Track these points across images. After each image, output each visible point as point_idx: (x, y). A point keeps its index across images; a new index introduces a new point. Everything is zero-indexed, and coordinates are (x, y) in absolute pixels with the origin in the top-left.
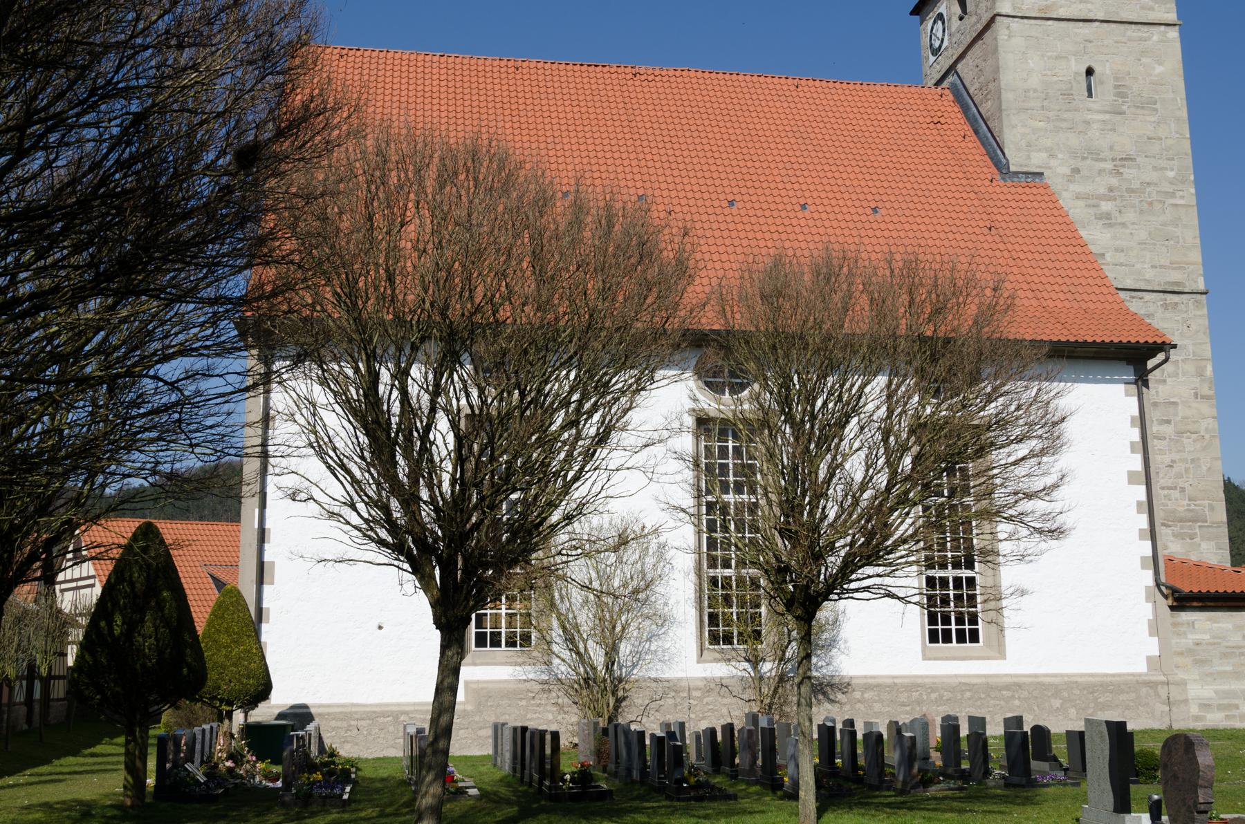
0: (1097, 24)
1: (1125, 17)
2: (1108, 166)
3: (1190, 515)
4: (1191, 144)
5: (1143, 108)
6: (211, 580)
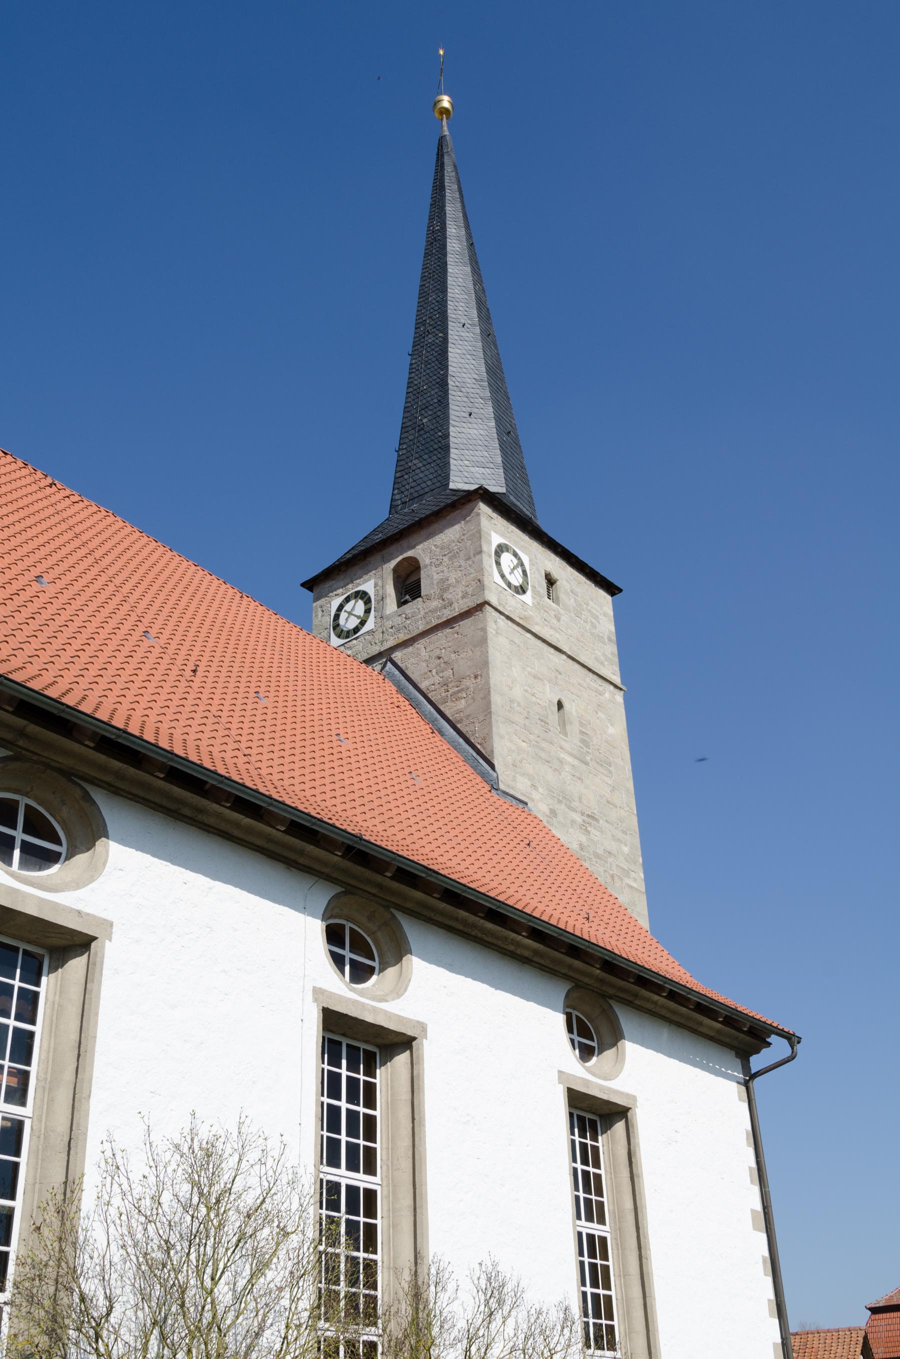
0: (564, 657)
1: (582, 659)
2: (578, 818)
3: (420, 1283)
5: (601, 765)
6: (861, 1340)
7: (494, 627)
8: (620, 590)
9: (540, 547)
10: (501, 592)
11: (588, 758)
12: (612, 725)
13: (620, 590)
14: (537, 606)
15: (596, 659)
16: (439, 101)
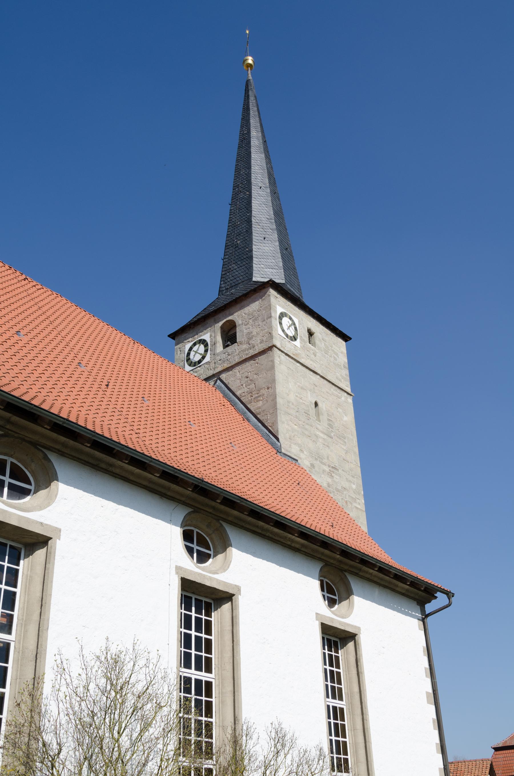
0: (318, 377)
3: (237, 735)
4: (361, 471)
5: (340, 438)
7: (279, 360)
8: (350, 339)
9: (305, 314)
11: (332, 434)
12: (346, 415)
13: (350, 339)
14: (303, 347)
15: (337, 378)
16: (247, 60)
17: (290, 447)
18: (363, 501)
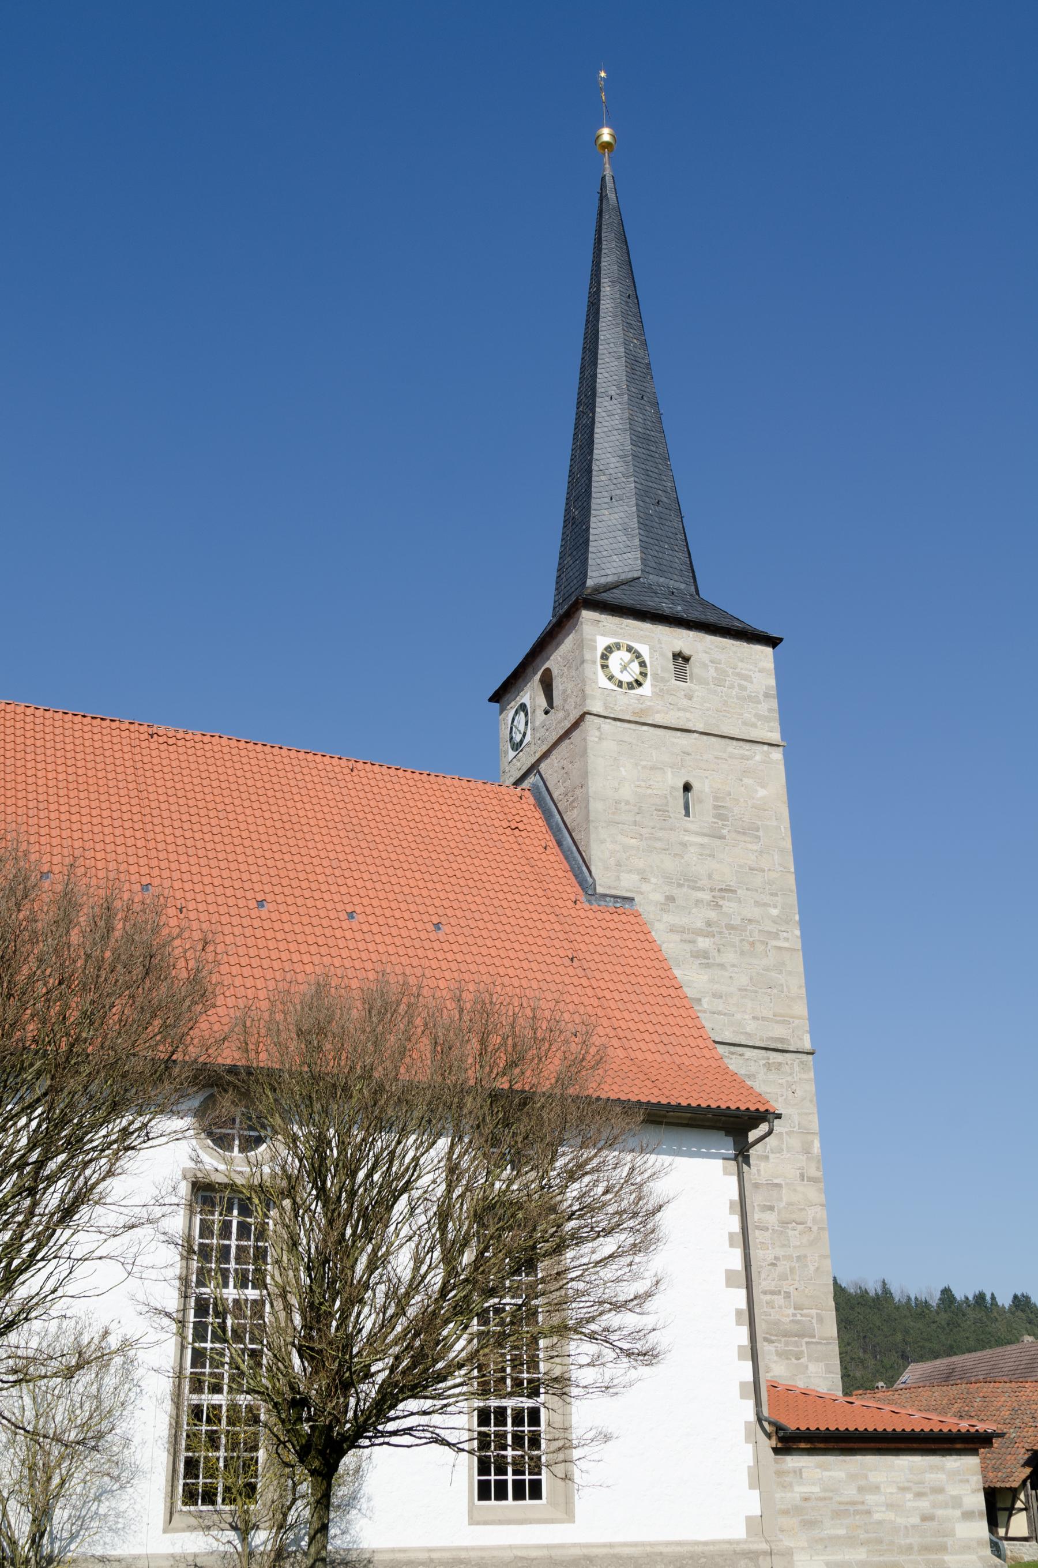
0: (696, 735)
5: (744, 834)
7: (597, 733)
8: (781, 640)
9: (667, 629)
10: (608, 695)
11: (724, 832)
12: (762, 787)
13: (781, 640)
14: (659, 694)
15: (745, 723)
16: (598, 137)
17: (618, 878)
18: (798, 933)
